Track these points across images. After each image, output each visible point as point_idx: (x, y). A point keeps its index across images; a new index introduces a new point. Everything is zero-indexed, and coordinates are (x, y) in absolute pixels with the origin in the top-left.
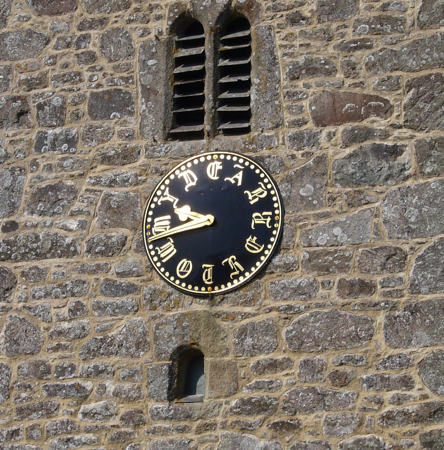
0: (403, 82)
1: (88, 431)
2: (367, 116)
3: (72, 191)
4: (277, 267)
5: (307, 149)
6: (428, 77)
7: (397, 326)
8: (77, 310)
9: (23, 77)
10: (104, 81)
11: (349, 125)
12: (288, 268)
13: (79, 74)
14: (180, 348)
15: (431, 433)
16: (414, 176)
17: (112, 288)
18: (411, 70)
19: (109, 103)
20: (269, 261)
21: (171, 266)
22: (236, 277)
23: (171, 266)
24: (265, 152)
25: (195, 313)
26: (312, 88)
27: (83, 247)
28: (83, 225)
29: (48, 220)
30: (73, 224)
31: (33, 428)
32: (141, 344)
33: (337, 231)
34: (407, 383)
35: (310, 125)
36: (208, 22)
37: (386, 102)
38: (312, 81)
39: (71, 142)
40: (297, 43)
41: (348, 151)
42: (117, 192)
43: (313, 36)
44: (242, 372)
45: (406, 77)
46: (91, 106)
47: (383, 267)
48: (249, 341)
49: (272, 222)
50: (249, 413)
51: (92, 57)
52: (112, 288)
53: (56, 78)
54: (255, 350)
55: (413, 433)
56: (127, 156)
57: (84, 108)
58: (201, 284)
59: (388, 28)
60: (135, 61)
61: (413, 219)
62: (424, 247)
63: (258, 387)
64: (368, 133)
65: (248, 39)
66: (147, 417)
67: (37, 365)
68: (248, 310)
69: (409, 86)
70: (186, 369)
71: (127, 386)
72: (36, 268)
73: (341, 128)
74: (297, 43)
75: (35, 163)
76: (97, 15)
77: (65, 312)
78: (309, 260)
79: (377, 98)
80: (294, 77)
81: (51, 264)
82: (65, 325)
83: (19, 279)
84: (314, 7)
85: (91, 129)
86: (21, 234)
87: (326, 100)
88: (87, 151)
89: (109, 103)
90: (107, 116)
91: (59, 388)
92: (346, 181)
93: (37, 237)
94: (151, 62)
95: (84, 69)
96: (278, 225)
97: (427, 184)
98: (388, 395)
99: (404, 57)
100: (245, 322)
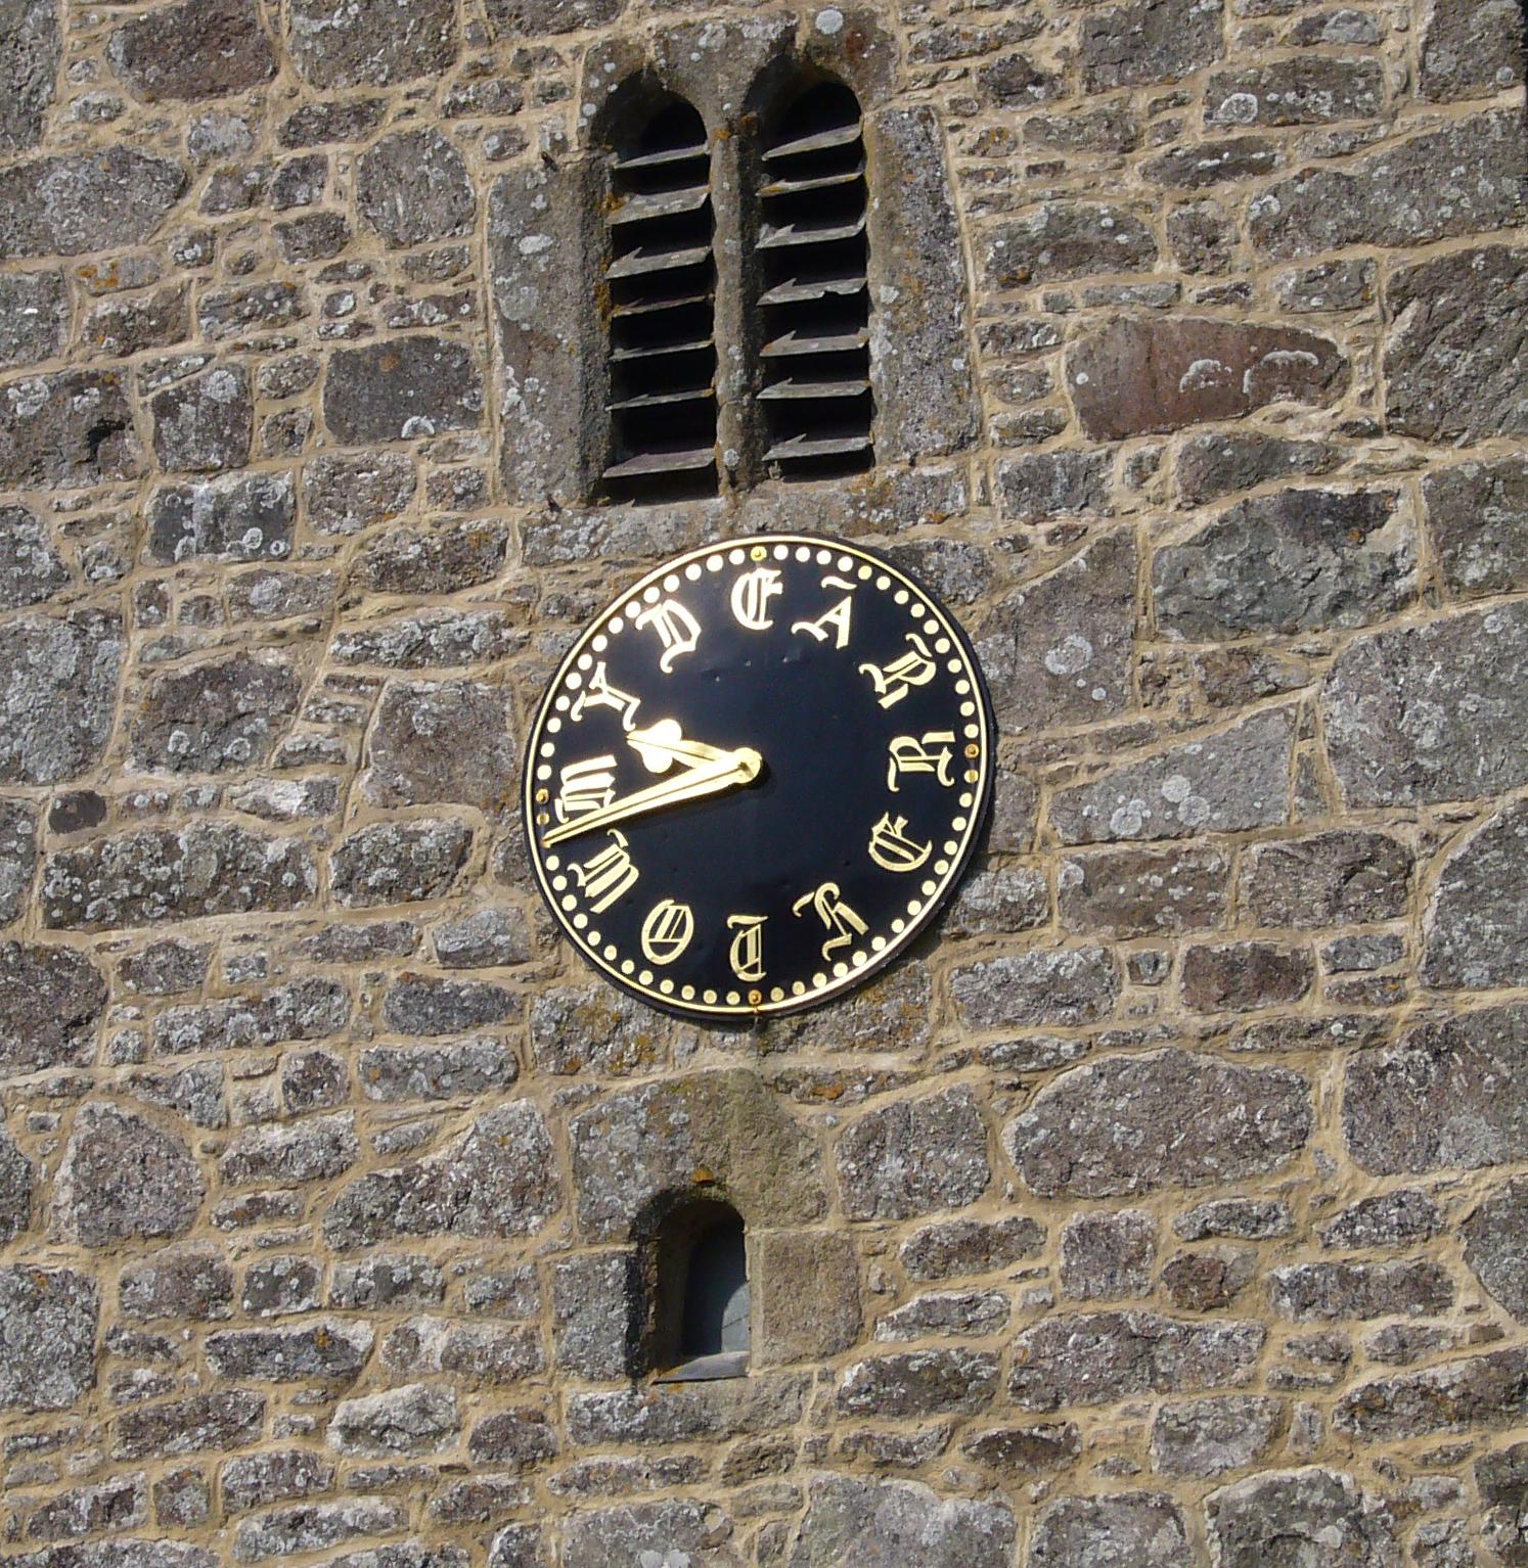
1: (363, 1488)
2: (1263, 398)
6: (1461, 262)
8: (312, 1084)
10: (375, 313)
11: (1203, 433)
12: (1016, 918)
13: (291, 291)
14: (663, 1199)
16: (1428, 593)
17: (426, 1006)
19: (399, 384)
20: (951, 896)
22: (843, 954)
23: (621, 924)
25: (709, 1079)
26: (1073, 312)
28: (321, 799)
29: (205, 783)
30: (289, 795)
33: (1175, 787)
34: (1428, 1289)
35: (1074, 435)
36: (719, 102)
38: (1074, 287)
39: (274, 520)
40: (1019, 162)
41: (1204, 518)
42: (433, 681)
43: (1070, 136)
45: (1387, 263)
47: (1335, 903)
48: (893, 1167)
49: (958, 767)
50: (902, 1410)
51: (332, 234)
52: (426, 1006)
53: (214, 308)
54: (913, 1196)
56: (462, 561)
57: (312, 404)
58: (725, 981)
59: (1324, 102)
61: (1428, 740)
62: (1470, 833)
63: (929, 1319)
66: (559, 1432)
67: (183, 1273)
68: (885, 1062)
69: (1401, 295)
72: (170, 946)
73: (1176, 443)
74: (1019, 162)
75: (153, 596)
76: (344, 93)
77: (271, 1090)
78: (1086, 889)
80: (1012, 277)
81: (220, 932)
82: (276, 1136)
83: (115, 987)
84: (1072, 40)
85: (338, 476)
86: (117, 836)
87: (1123, 351)
88: (329, 548)
89: (399, 384)
91: (263, 1347)
92: (1198, 618)
93: (170, 844)
94: (530, 244)
96: (976, 776)
98: (1365, 1334)
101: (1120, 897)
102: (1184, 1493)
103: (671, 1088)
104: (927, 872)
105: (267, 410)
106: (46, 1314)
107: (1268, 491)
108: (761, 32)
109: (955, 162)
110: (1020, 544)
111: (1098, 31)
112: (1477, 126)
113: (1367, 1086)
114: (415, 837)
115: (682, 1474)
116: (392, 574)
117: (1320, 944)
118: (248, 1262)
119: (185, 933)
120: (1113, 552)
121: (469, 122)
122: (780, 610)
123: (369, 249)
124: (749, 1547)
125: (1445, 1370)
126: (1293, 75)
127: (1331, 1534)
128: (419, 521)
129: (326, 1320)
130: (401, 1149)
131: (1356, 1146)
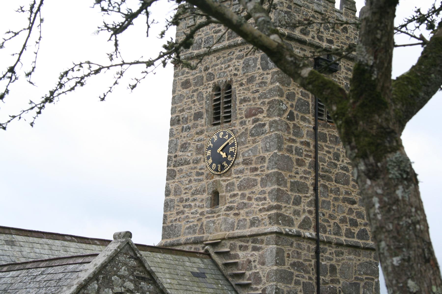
0: (266, 103)
1: (192, 218)
2: (258, 114)
3: (189, 144)
4: (236, 164)
5: (243, 126)
6: (272, 100)
7: (263, 181)
8: (190, 181)
9: (179, 109)
10: (197, 109)
11: (253, 118)
12: (238, 164)
13: (191, 107)
14: (213, 191)
15: (270, 214)
16: (269, 133)
17: (198, 174)
18: (268, 98)
19: (198, 116)
20: (234, 162)
21: (211, 166)
22: (226, 168)
23: (211, 166)
24: (233, 128)
25: (216, 180)
26: (245, 107)
27: (191, 161)
28: (192, 154)
29: (184, 153)
30: (189, 154)
31: (180, 218)
32: (204, 191)
33: (250, 152)
34: (265, 199)
35: (244, 119)
36: (222, 87)
37: (262, 109)
38: (245, 104)
39: (189, 128)
40: (242, 92)
41: (253, 126)
42: (199, 143)
43: (245, 89)
44: (227, 198)
45: (267, 100)
46: (194, 117)
47: (261, 162)
48: (229, 188)
49: (234, 150)
50: (228, 211)
51: (194, 102)
52: (198, 174)
53: (187, 109)
54: (230, 191)
55: (266, 214)
56: (202, 132)
57: (192, 118)
58: (217, 171)
59: (263, 85)
60: (204, 102)
61: (268, 147)
62: (271, 155)
63: (231, 202)
64: (258, 120)
65: (230, 112)
66: (205, 213)
67: (181, 198)
68: (229, 178)
69: (268, 103)
70: (216, 198)
71: (201, 204)
72: (181, 169)
73: (252, 119)
74: (242, 92)
75: (181, 136)
76: (196, 88)
77: (187, 182)
78: (243, 161)
79: (260, 108)
80: (241, 103)
81: (184, 167)
82: (188, 186)
83: (177, 172)
84: (246, 80)
85: (194, 124)
86: (178, 158)
87: (248, 110)
88: (193, 131)
89: (198, 116)
90: (197, 120)
91: (186, 205)
92: (252, 135)
93: (181, 159)
94: (208, 102)
95: (192, 105)
96: (236, 151)
97: (271, 135)
98: (260, 203)
99: (267, 94)
100: (229, 182)
101: (246, 162)
102: (247, 218)
103: (214, 181)
104: (232, 160)
105: (189, 118)
106: (172, 203)
107: (257, 123)
108: (224, 80)
109: (238, 92)
110: (240, 129)
111: (248, 79)
112: (274, 87)
113: (262, 179)
114: (197, 158)
115: (213, 217)
116: (197, 133)
117: (259, 166)
118: (186, 198)
119: (182, 167)
120: (246, 130)
121: (204, 90)
122: (223, 136)
123: (197, 103)
124: (213, 230)
125: (266, 206)
126: (262, 83)
127: (257, 222)
128: (199, 128)
129: (190, 203)
130: (196, 187)
131: (261, 186)
